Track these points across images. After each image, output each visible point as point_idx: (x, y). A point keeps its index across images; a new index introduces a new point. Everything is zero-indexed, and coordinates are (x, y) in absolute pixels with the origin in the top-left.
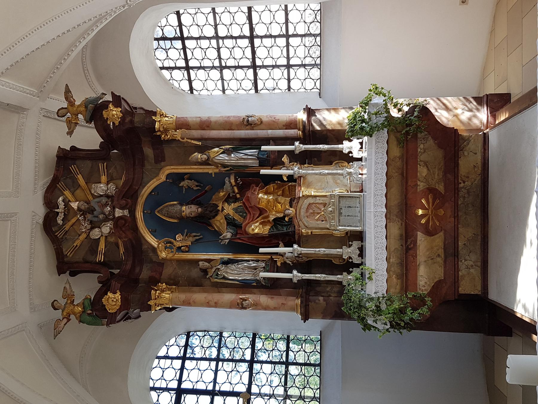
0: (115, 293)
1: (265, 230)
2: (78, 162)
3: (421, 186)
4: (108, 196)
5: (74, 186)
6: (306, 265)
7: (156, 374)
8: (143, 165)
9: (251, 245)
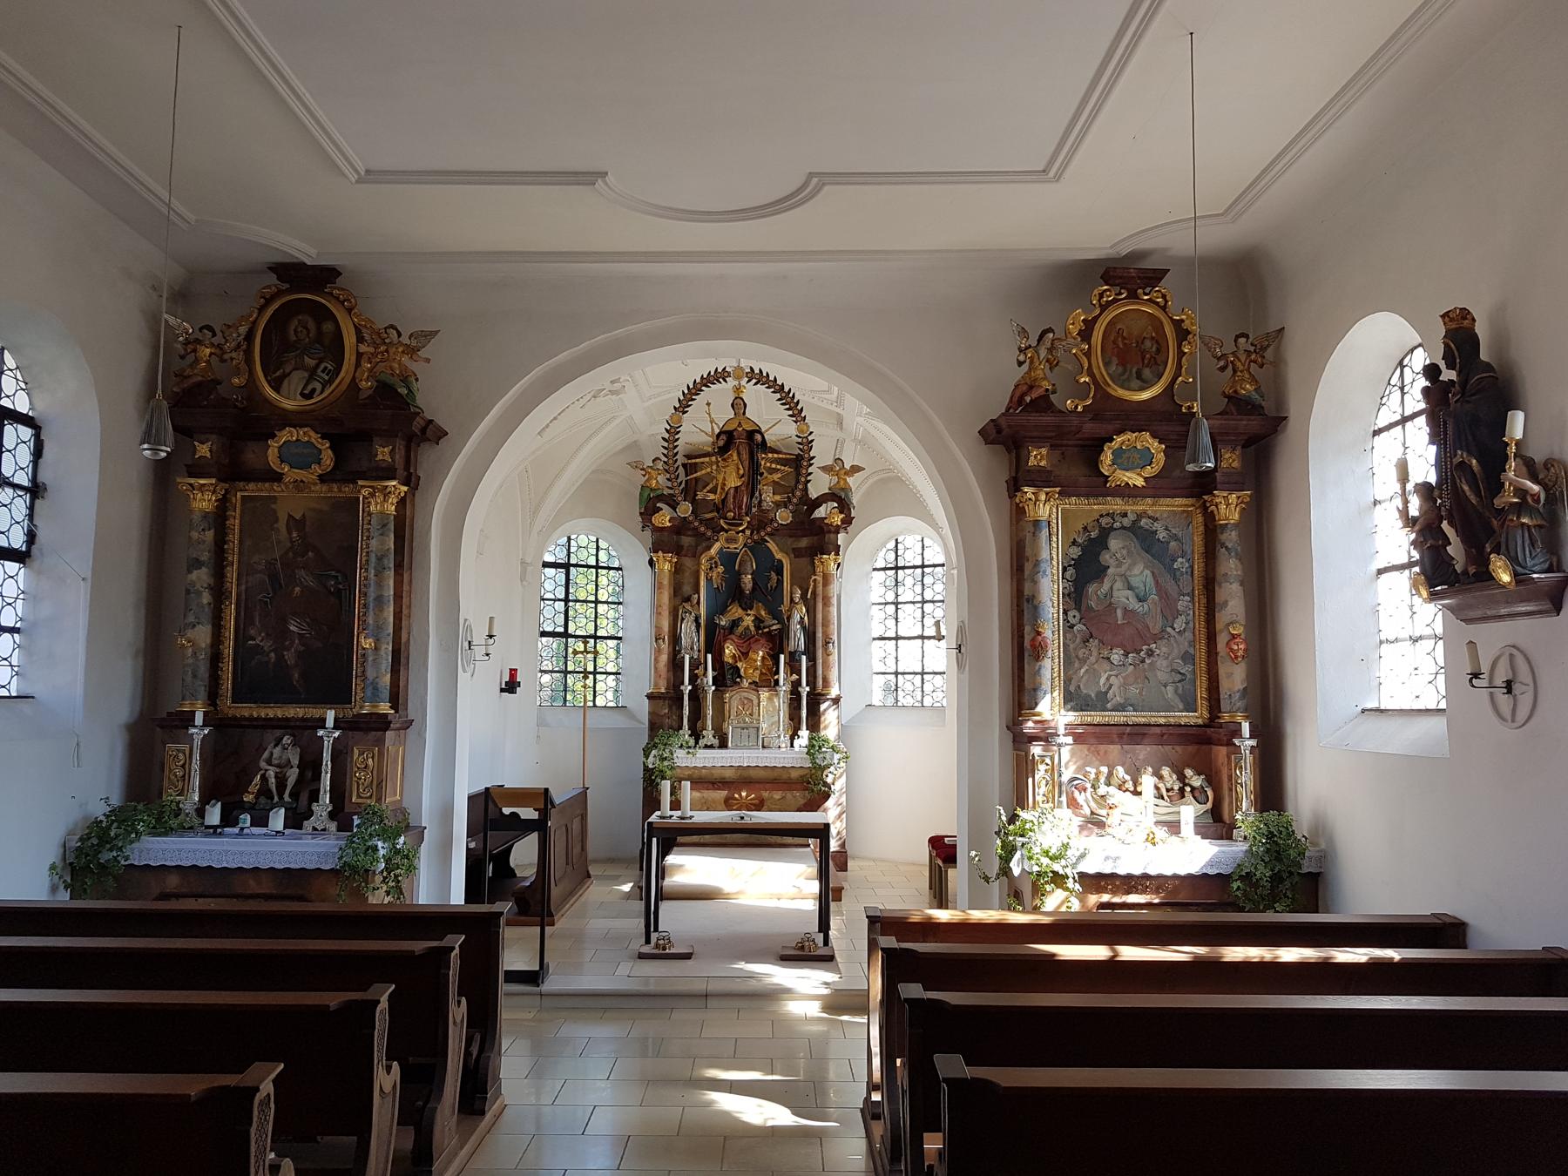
1: (728, 659)
3: (765, 794)
6: (696, 697)
7: (583, 540)
9: (713, 645)
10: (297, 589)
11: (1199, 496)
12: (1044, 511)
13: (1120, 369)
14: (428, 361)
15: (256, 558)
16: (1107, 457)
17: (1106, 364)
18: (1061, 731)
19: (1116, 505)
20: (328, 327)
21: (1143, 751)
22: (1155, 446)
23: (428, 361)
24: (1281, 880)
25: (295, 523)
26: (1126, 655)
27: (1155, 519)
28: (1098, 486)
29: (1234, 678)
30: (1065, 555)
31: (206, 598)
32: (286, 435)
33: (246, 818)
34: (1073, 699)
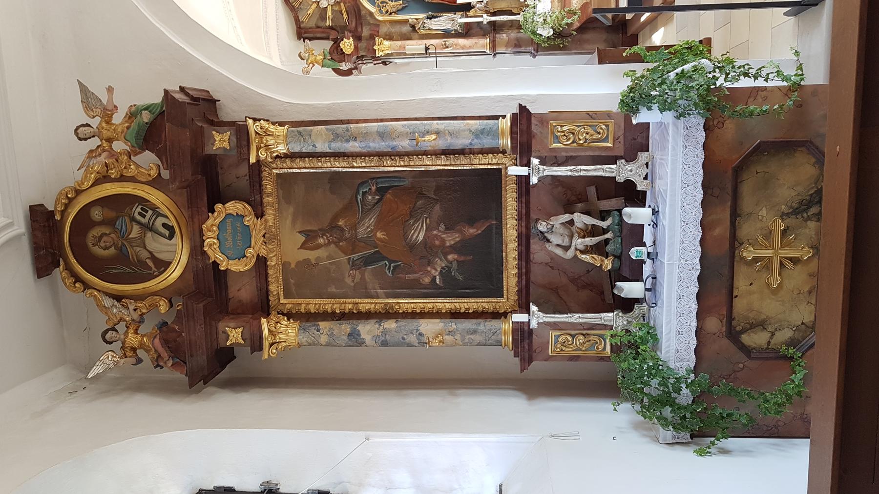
0: (349, 39)
10: (379, 235)
14: (110, 90)
15: (348, 281)
20: (97, 214)
23: (110, 90)
25: (310, 239)
31: (391, 324)
32: (215, 254)
33: (635, 253)
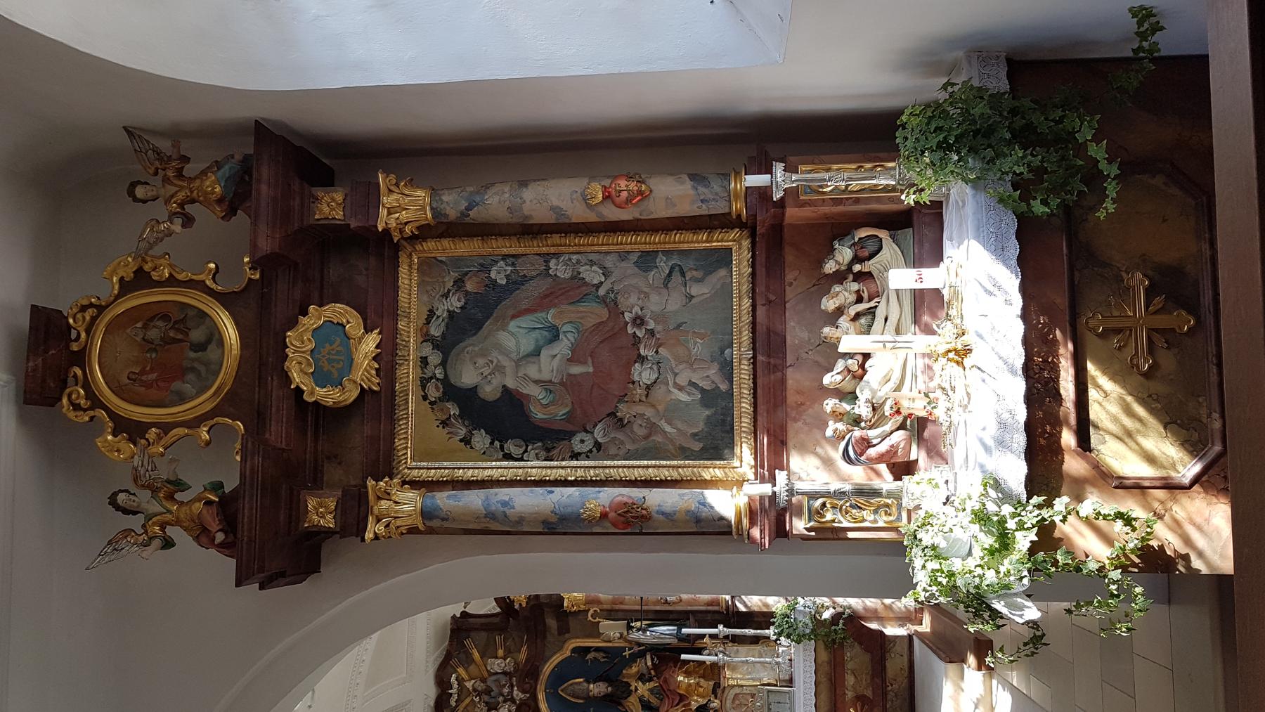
2: (473, 634)
4: (504, 673)
5: (468, 661)
8: (545, 637)
11: (396, 248)
12: (408, 502)
13: (190, 376)
16: (329, 396)
17: (182, 398)
18: (766, 489)
19: (408, 374)
21: (795, 333)
22: (315, 318)
24: (1030, 127)
26: (642, 359)
27: (431, 313)
28: (378, 404)
29: (672, 194)
30: (485, 456)
34: (717, 445)
